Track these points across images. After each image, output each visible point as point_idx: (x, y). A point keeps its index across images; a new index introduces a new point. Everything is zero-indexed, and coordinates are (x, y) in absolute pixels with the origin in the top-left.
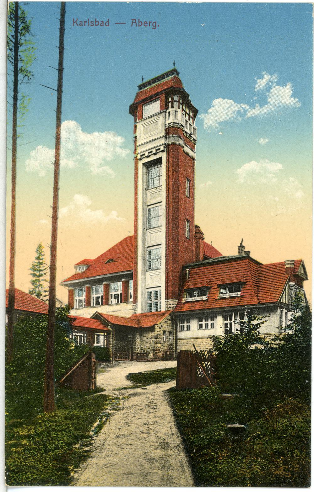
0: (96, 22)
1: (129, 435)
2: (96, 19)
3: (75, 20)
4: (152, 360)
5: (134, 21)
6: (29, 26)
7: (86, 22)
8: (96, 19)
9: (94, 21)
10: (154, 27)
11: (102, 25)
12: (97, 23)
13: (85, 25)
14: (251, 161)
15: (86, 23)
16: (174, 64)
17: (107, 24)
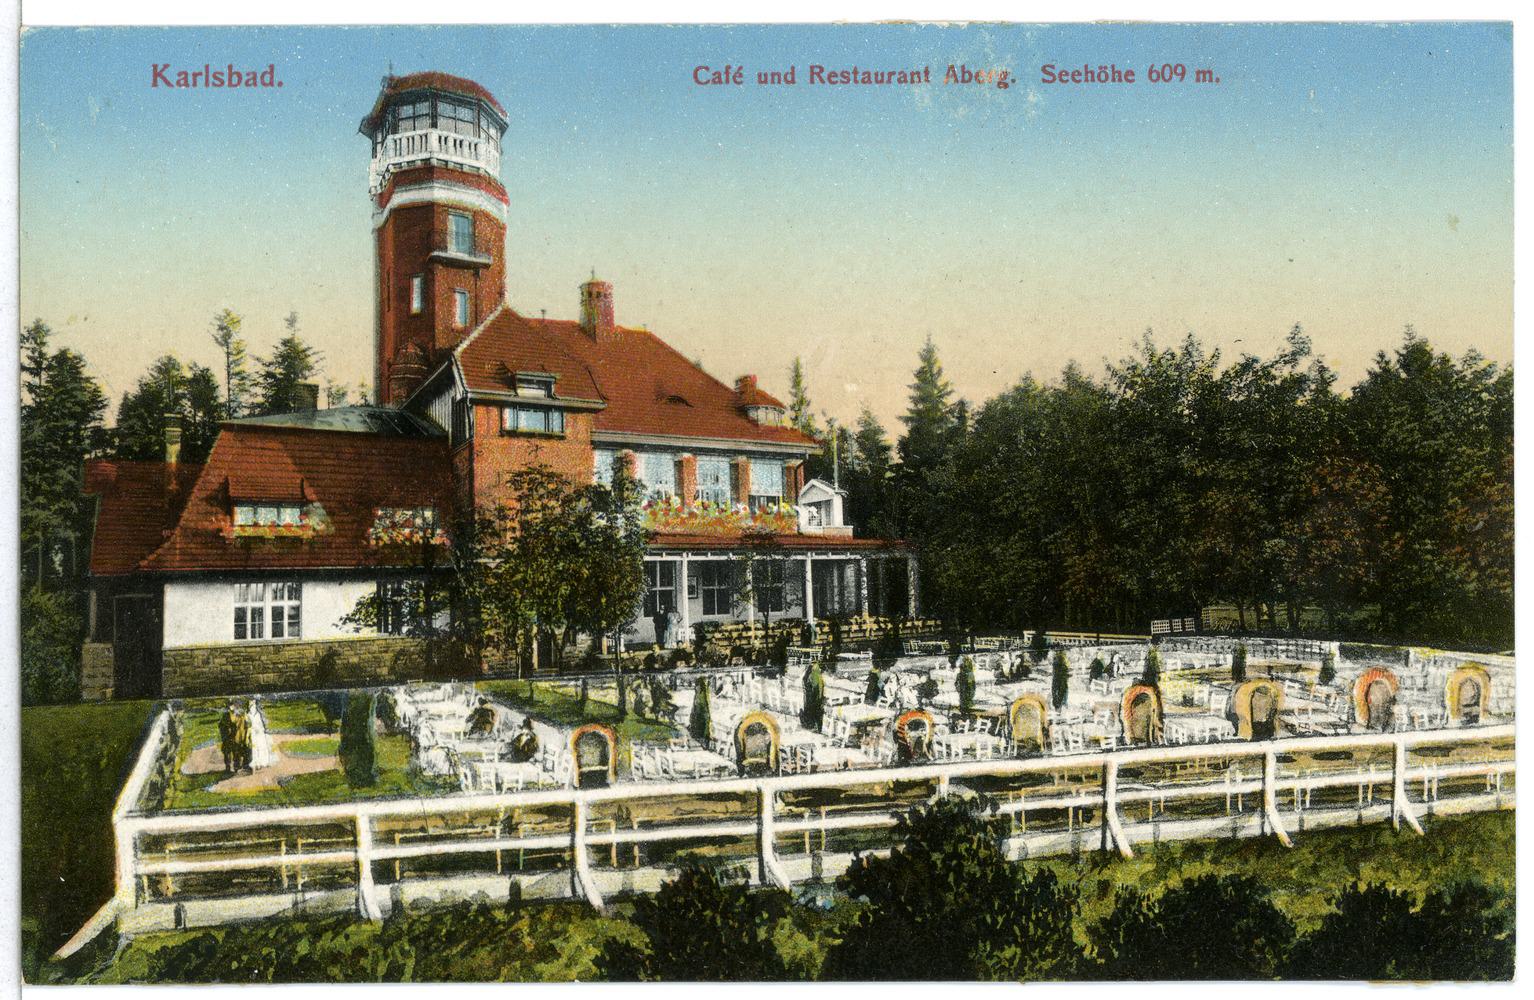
7: (200, 74)
9: (226, 71)
13: (195, 84)
15: (198, 78)
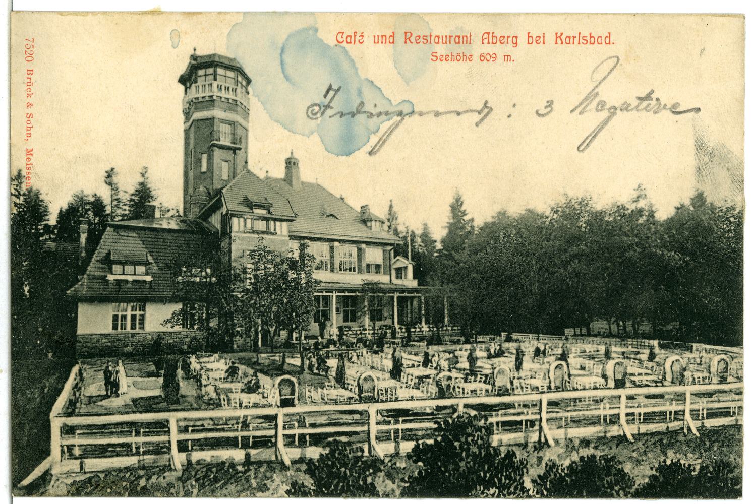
0: (591, 37)
1: (79, 385)
2: (590, 34)
3: (559, 35)
4: (188, 440)
5: (558, 37)
6: (317, 26)
8: (590, 34)
10: (515, 45)
11: (538, 39)
12: (592, 39)
14: (311, 185)
16: (195, 50)
17: (607, 41)
